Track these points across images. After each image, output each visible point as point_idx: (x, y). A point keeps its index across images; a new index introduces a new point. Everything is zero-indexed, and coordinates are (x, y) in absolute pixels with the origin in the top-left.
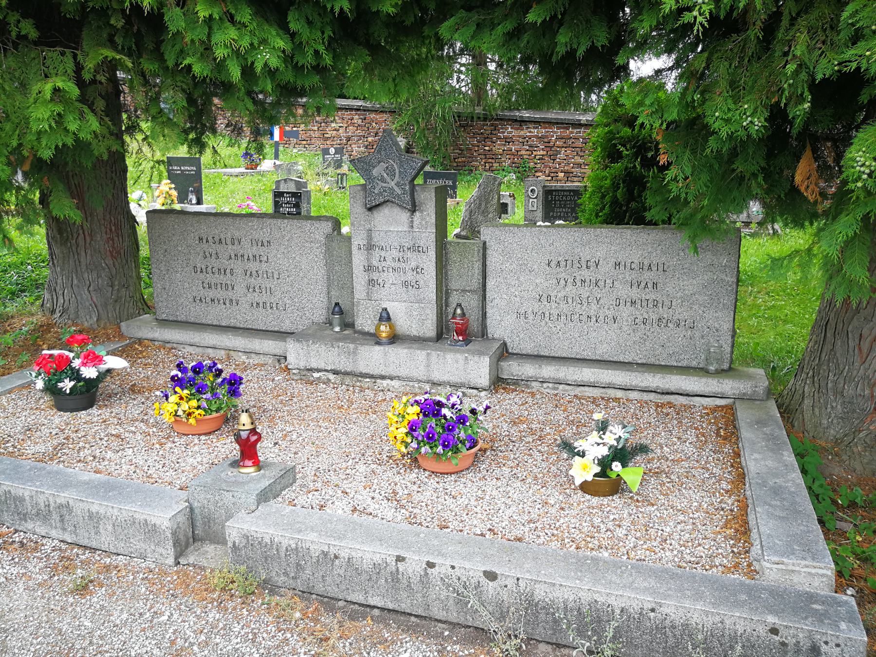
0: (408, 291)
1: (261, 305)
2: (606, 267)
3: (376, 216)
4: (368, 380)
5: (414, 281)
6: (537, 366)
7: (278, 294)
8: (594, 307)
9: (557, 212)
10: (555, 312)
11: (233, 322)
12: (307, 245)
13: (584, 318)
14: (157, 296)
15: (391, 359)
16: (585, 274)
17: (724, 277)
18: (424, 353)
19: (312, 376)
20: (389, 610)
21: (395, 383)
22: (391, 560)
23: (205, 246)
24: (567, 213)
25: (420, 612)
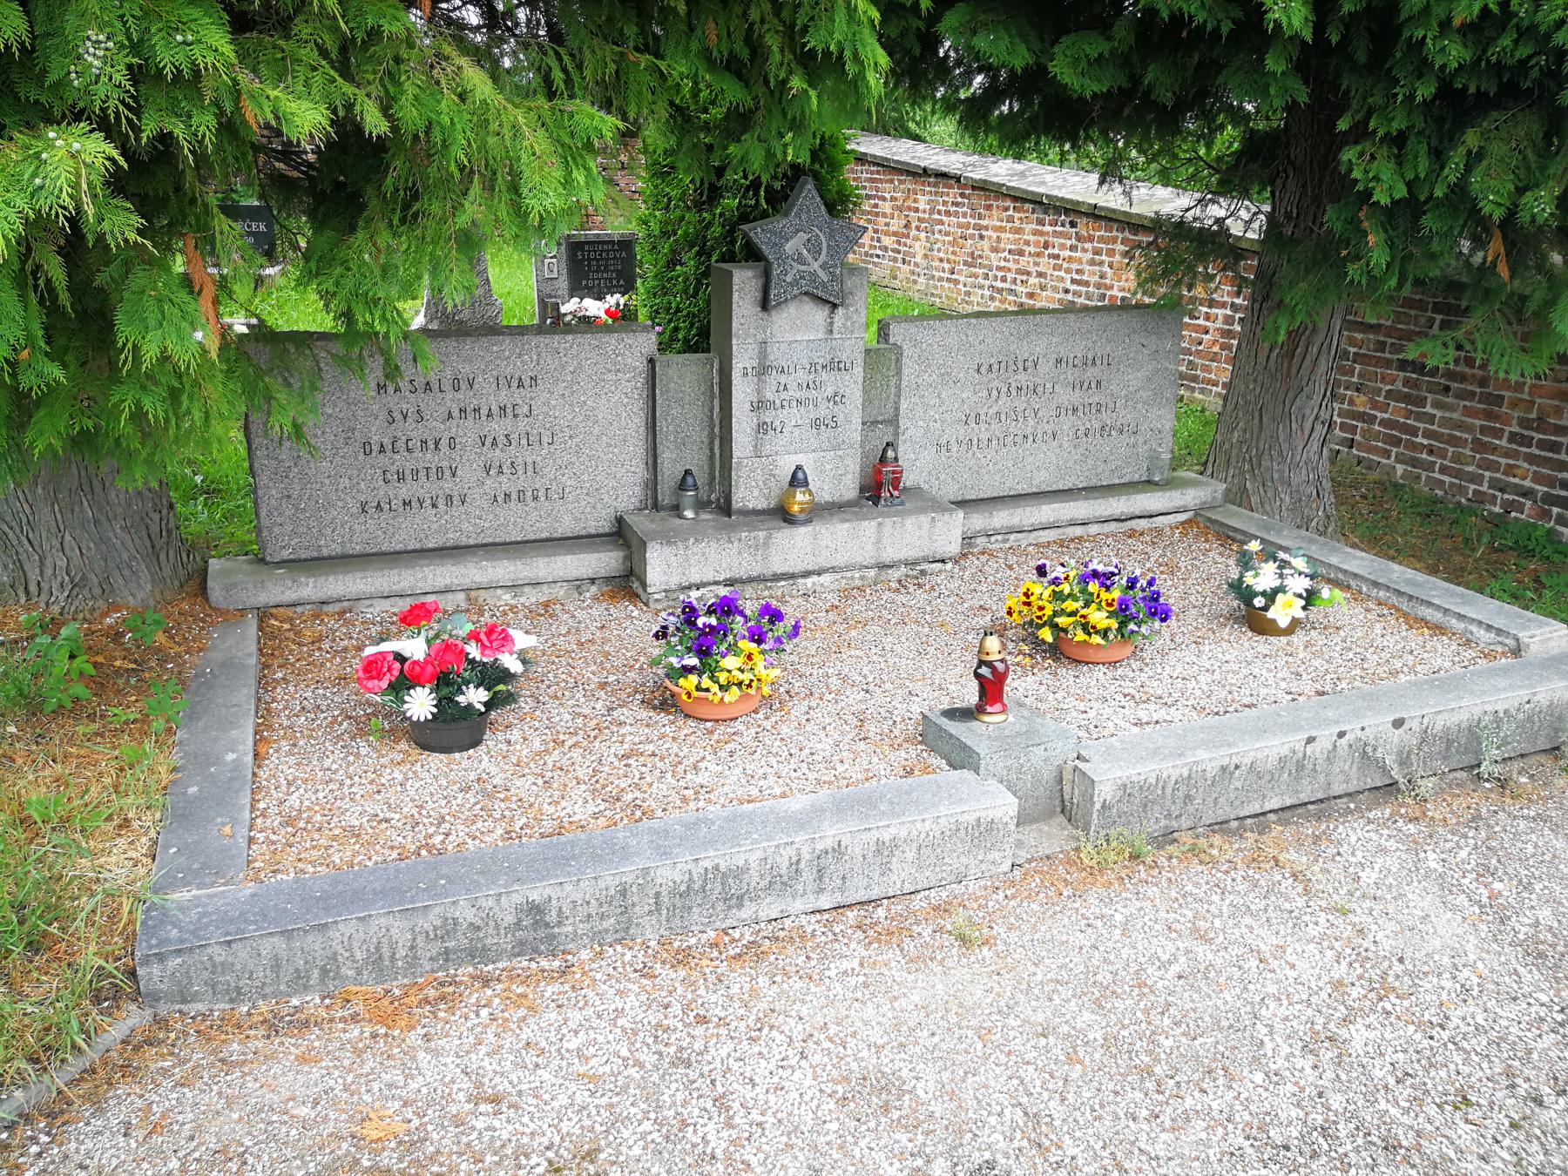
0: (818, 434)
1: (514, 496)
2: (1045, 367)
3: (774, 318)
4: (783, 583)
7: (550, 472)
8: (1031, 422)
10: (984, 436)
11: (452, 538)
12: (609, 377)
13: (1019, 439)
14: (270, 513)
17: (1167, 365)
18: (874, 523)
20: (1289, 808)
21: (826, 579)
22: (1299, 747)
25: (1320, 796)
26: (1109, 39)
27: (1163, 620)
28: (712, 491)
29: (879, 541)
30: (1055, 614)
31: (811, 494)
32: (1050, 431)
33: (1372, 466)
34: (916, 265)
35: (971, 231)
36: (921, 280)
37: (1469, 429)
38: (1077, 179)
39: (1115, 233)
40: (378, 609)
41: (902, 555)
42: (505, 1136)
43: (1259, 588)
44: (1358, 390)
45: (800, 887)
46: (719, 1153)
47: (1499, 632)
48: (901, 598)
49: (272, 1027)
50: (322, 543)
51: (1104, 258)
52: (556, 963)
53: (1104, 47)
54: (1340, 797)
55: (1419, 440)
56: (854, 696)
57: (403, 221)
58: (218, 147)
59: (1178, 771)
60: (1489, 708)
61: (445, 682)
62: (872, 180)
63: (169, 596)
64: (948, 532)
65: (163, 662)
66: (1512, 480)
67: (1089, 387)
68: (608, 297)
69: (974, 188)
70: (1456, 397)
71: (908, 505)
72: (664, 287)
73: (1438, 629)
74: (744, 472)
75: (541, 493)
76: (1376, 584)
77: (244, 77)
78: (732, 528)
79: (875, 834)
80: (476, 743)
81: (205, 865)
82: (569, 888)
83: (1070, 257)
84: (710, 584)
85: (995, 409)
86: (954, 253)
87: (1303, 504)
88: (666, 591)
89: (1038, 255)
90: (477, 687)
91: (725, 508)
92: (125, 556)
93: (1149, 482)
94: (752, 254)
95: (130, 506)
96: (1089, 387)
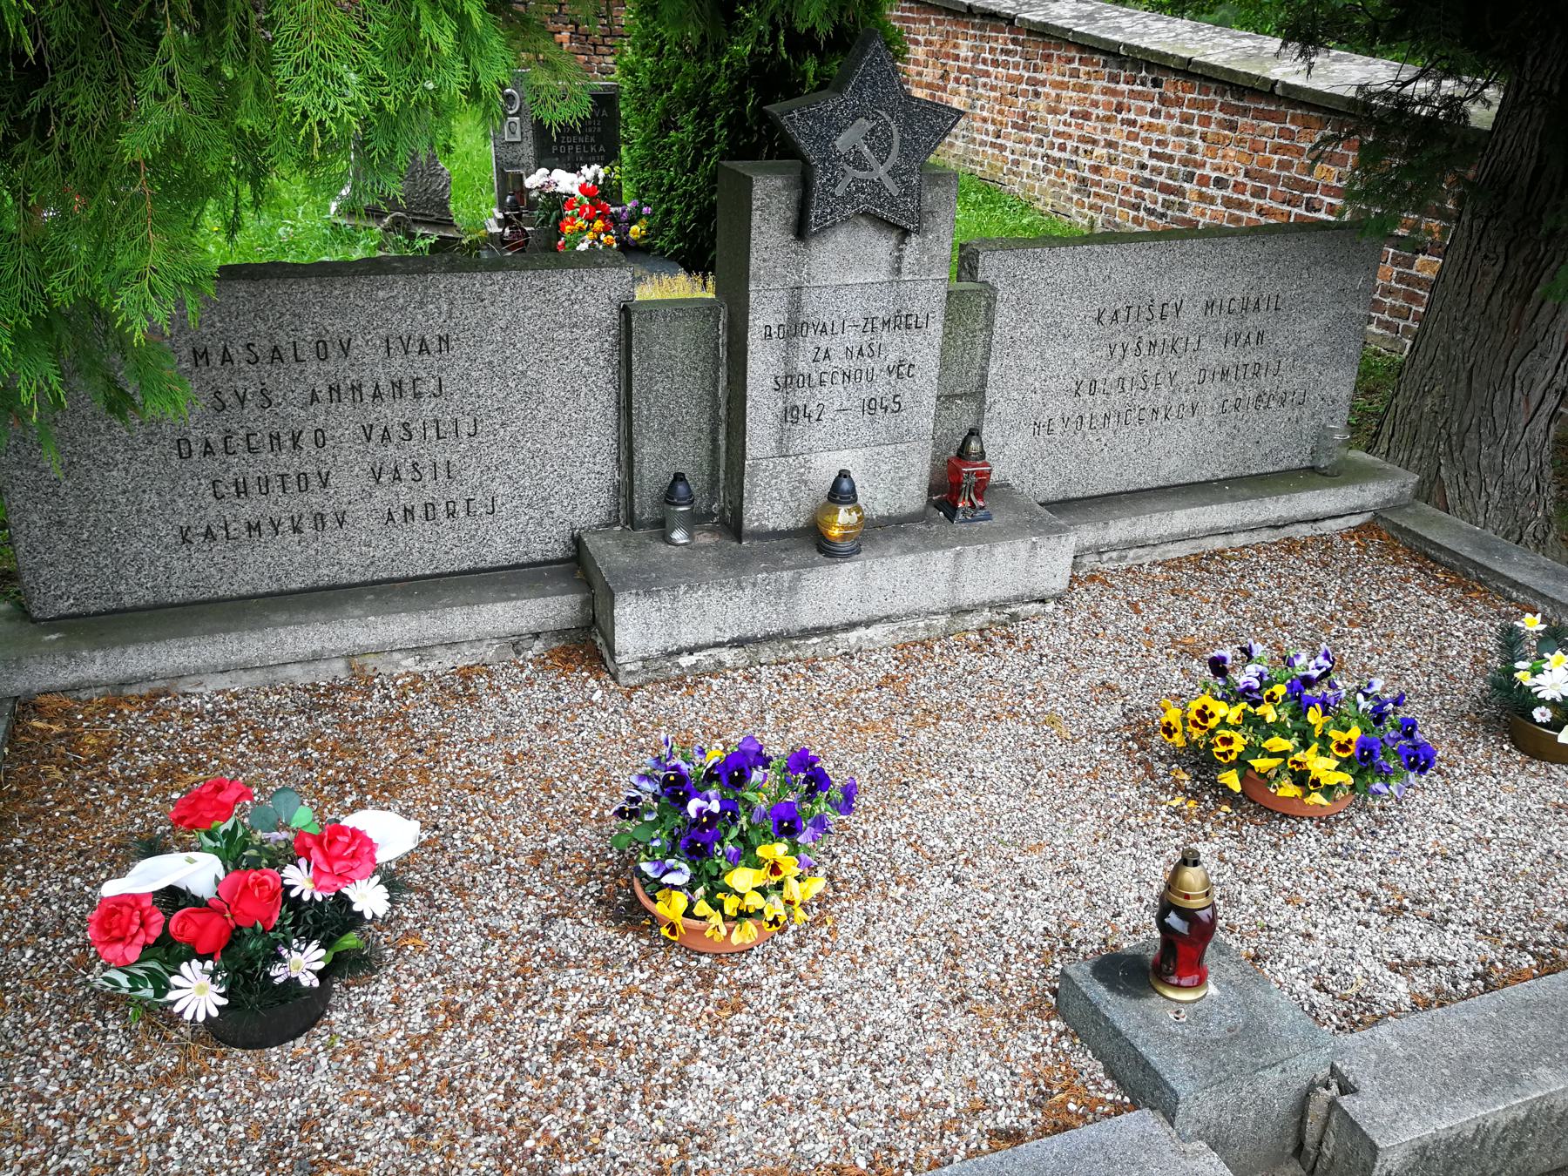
1: (419, 512)
2: (1191, 314)
3: (814, 251)
4: (815, 640)
5: (890, 396)
6: (1101, 524)
7: (472, 475)
8: (1164, 391)
9: (566, 145)
10: (1100, 411)
11: (326, 575)
12: (561, 335)
13: (1146, 415)
16: (1159, 330)
18: (950, 554)
19: (679, 666)
21: (877, 632)
23: (217, 373)
28: (713, 499)
29: (955, 578)
31: (858, 509)
35: (1024, 86)
38: (1160, 25)
39: (1212, 96)
40: (210, 687)
41: (986, 596)
43: (1547, 694)
48: (987, 664)
50: (122, 588)
51: (1195, 127)
67: (1247, 342)
69: (1030, 32)
71: (997, 520)
72: (654, 158)
74: (762, 478)
75: (460, 507)
83: (1150, 125)
84: (708, 647)
85: (1118, 373)
86: (1001, 112)
87: (1517, 501)
88: (643, 659)
89: (1108, 119)
91: (732, 526)
93: (1312, 469)
94: (780, 149)
96: (1247, 342)
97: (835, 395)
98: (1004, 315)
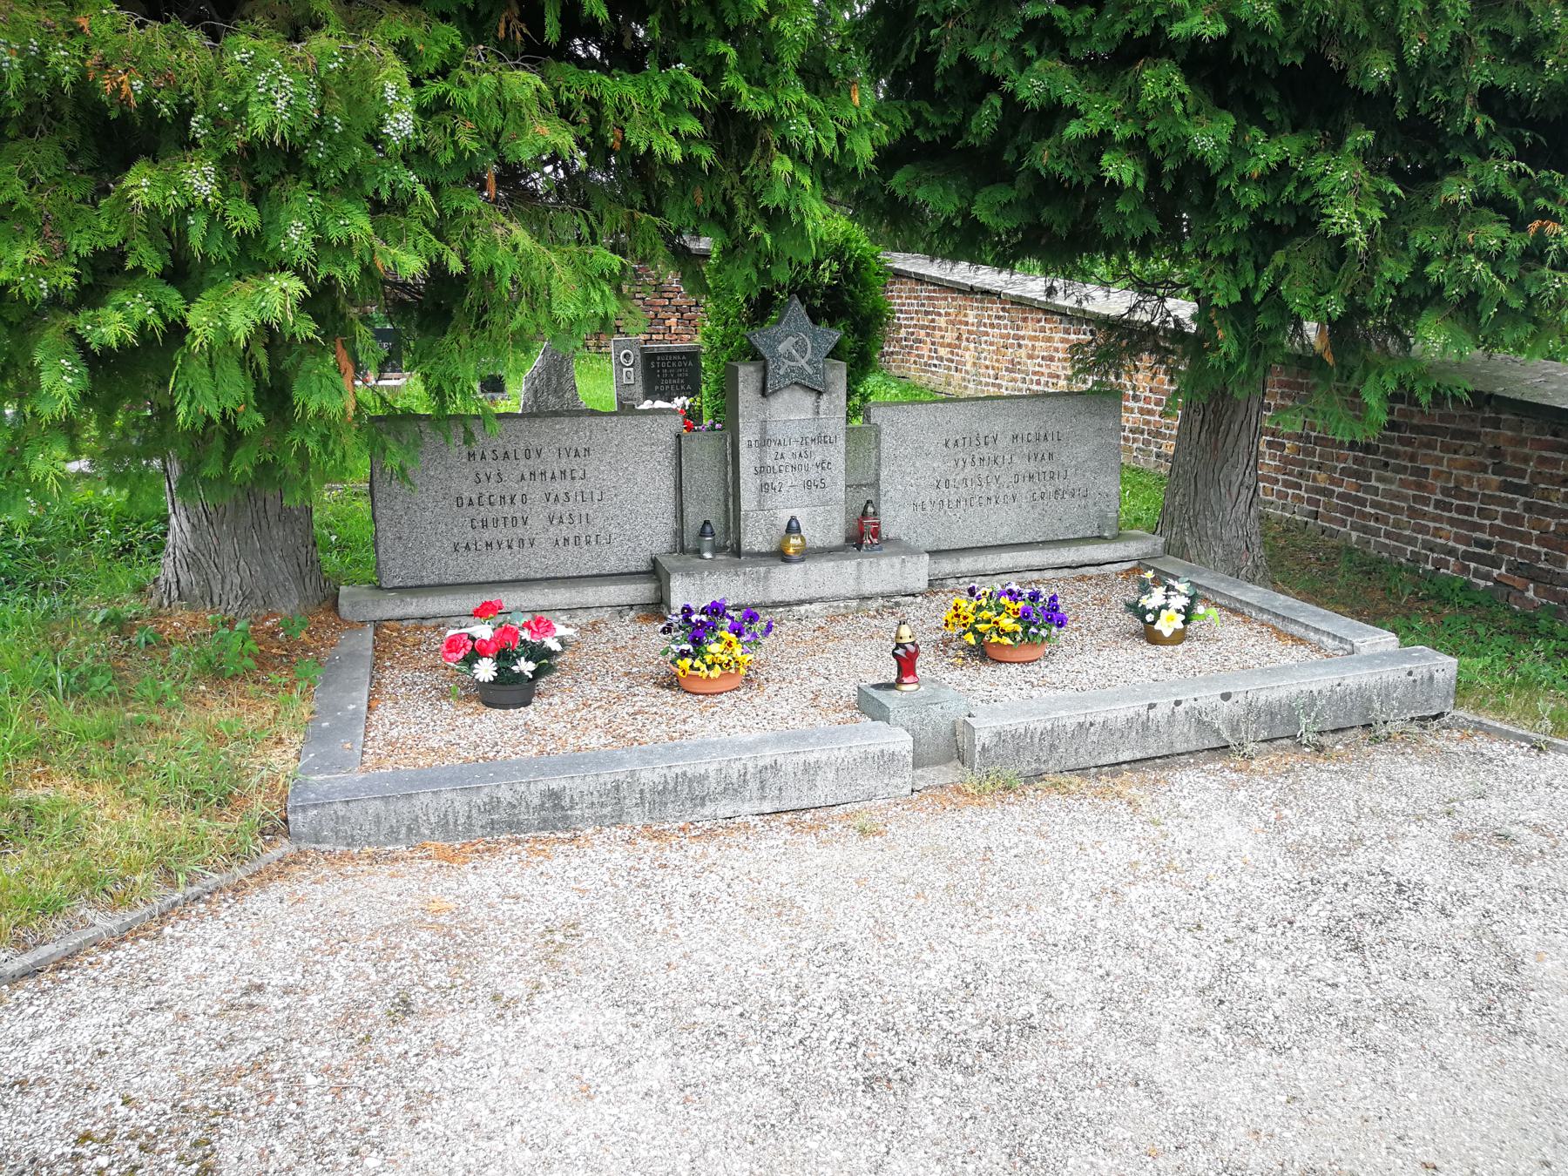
1: (572, 540)
2: (1004, 442)
7: (599, 522)
8: (994, 487)
10: (954, 498)
11: (523, 573)
12: (645, 449)
13: (984, 501)
15: (813, 578)
16: (984, 450)
18: (854, 563)
21: (816, 607)
22: (1143, 711)
23: (478, 464)
24: (679, 386)
25: (1165, 752)
26: (1012, 186)
27: (1059, 626)
30: (977, 622)
31: (803, 539)
32: (1010, 495)
33: (1334, 534)
34: (967, 372)
36: (971, 385)
37: (1404, 498)
41: (878, 589)
42: (520, 914)
43: (1149, 607)
44: (1319, 468)
45: (747, 794)
46: (660, 930)
47: (1341, 640)
49: (374, 859)
52: (568, 835)
53: (1013, 194)
54: (1182, 754)
55: (1368, 509)
56: (817, 682)
57: (476, 327)
58: (360, 283)
59: (1042, 725)
60: (1304, 688)
61: (504, 657)
62: (929, 298)
63: (310, 609)
64: (917, 572)
65: (305, 651)
66: (1438, 540)
68: (676, 399)
69: (1012, 303)
70: (1393, 471)
71: (885, 550)
73: (1299, 641)
75: (593, 539)
76: (1261, 610)
77: (377, 243)
78: (741, 565)
79: (802, 757)
80: (527, 703)
81: (332, 764)
82: (578, 781)
86: (997, 361)
90: (527, 660)
91: (737, 552)
92: (281, 578)
93: (1099, 537)
94: (754, 355)
95: (286, 540)
97: (788, 478)
98: (887, 443)
